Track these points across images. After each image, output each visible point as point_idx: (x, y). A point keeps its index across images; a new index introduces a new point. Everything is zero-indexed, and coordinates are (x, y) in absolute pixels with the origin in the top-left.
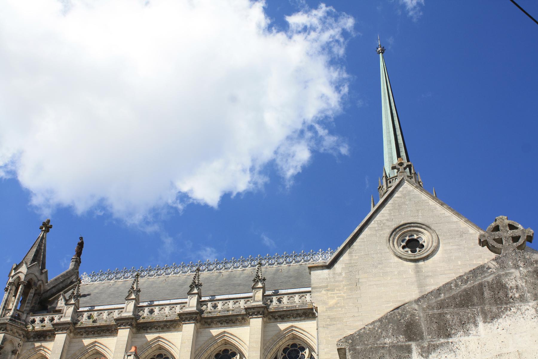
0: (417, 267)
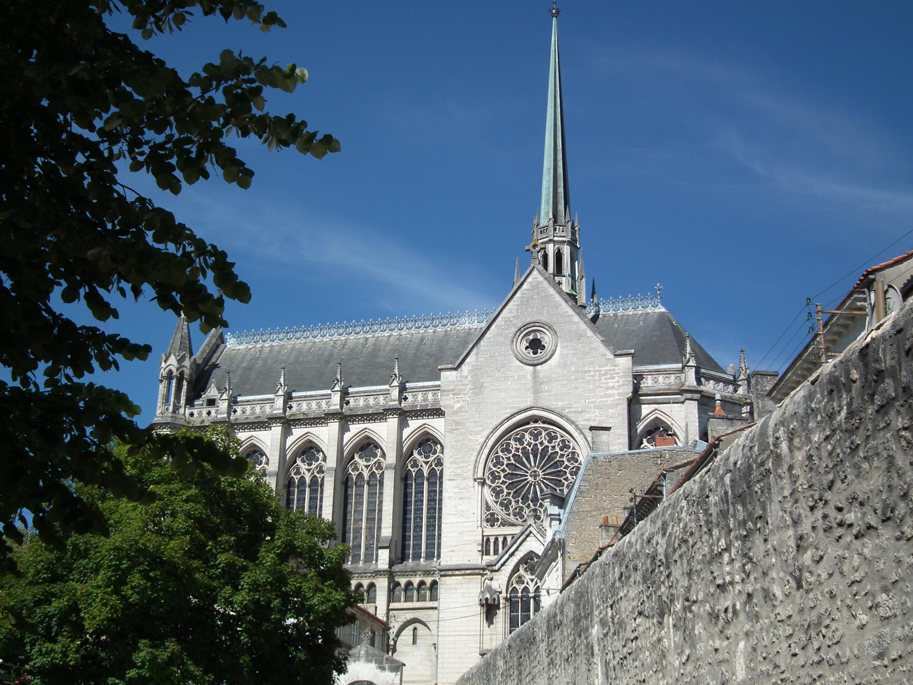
0: (535, 372)
